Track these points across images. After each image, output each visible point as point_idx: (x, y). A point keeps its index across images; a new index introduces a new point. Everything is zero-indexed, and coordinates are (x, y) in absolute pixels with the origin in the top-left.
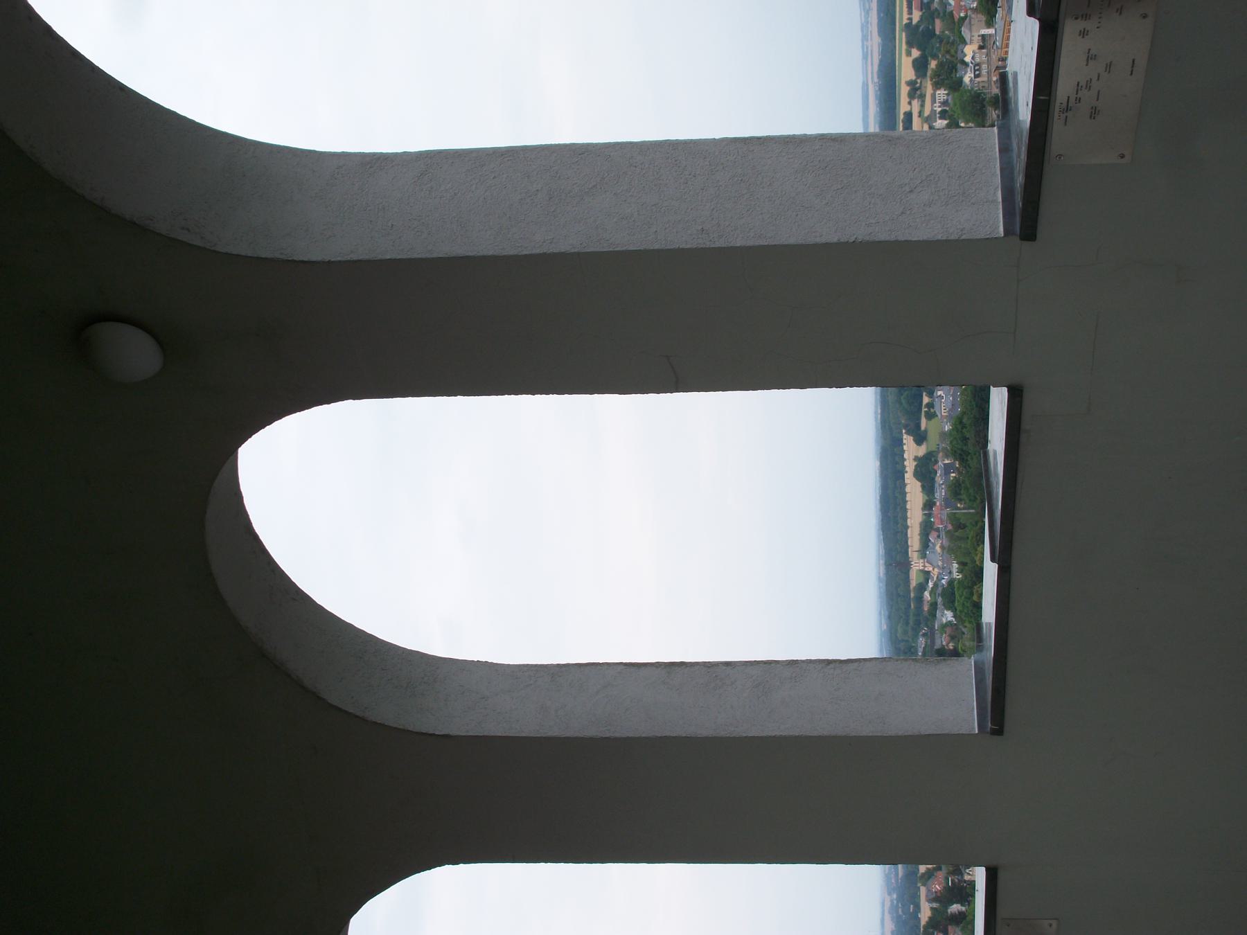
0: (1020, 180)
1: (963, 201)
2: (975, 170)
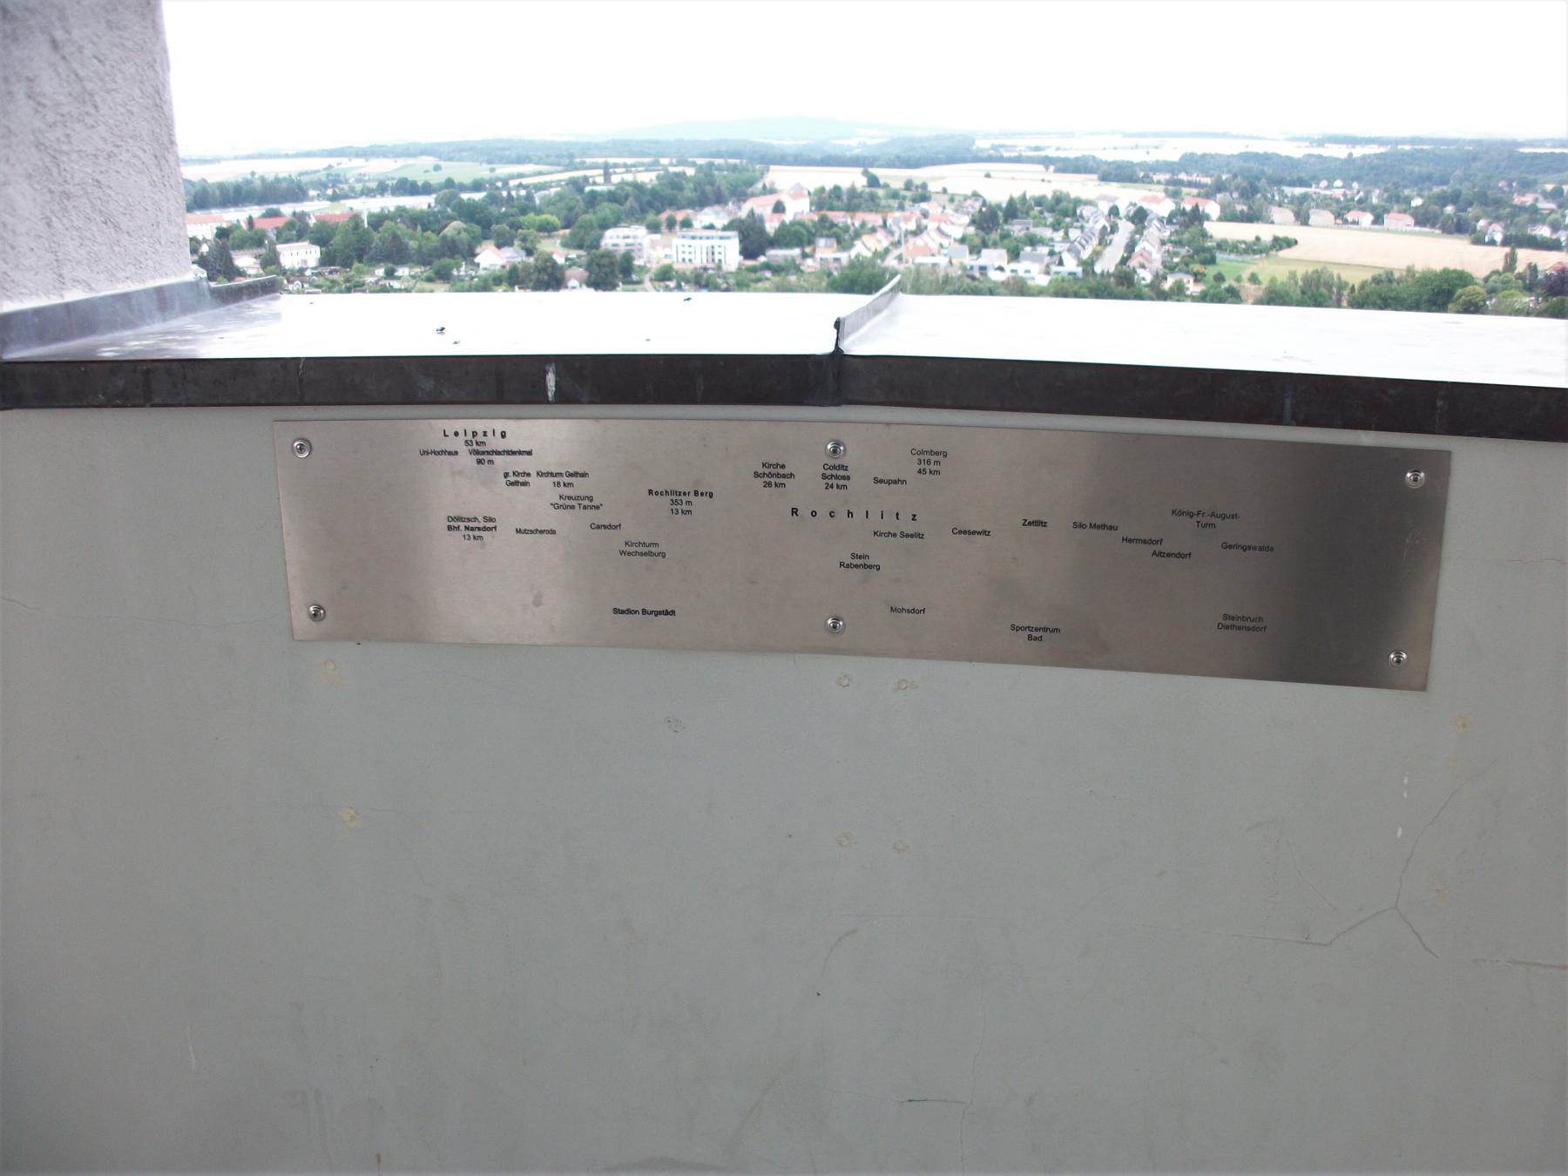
0: (113, 345)
1: (51, 192)
2: (117, 227)
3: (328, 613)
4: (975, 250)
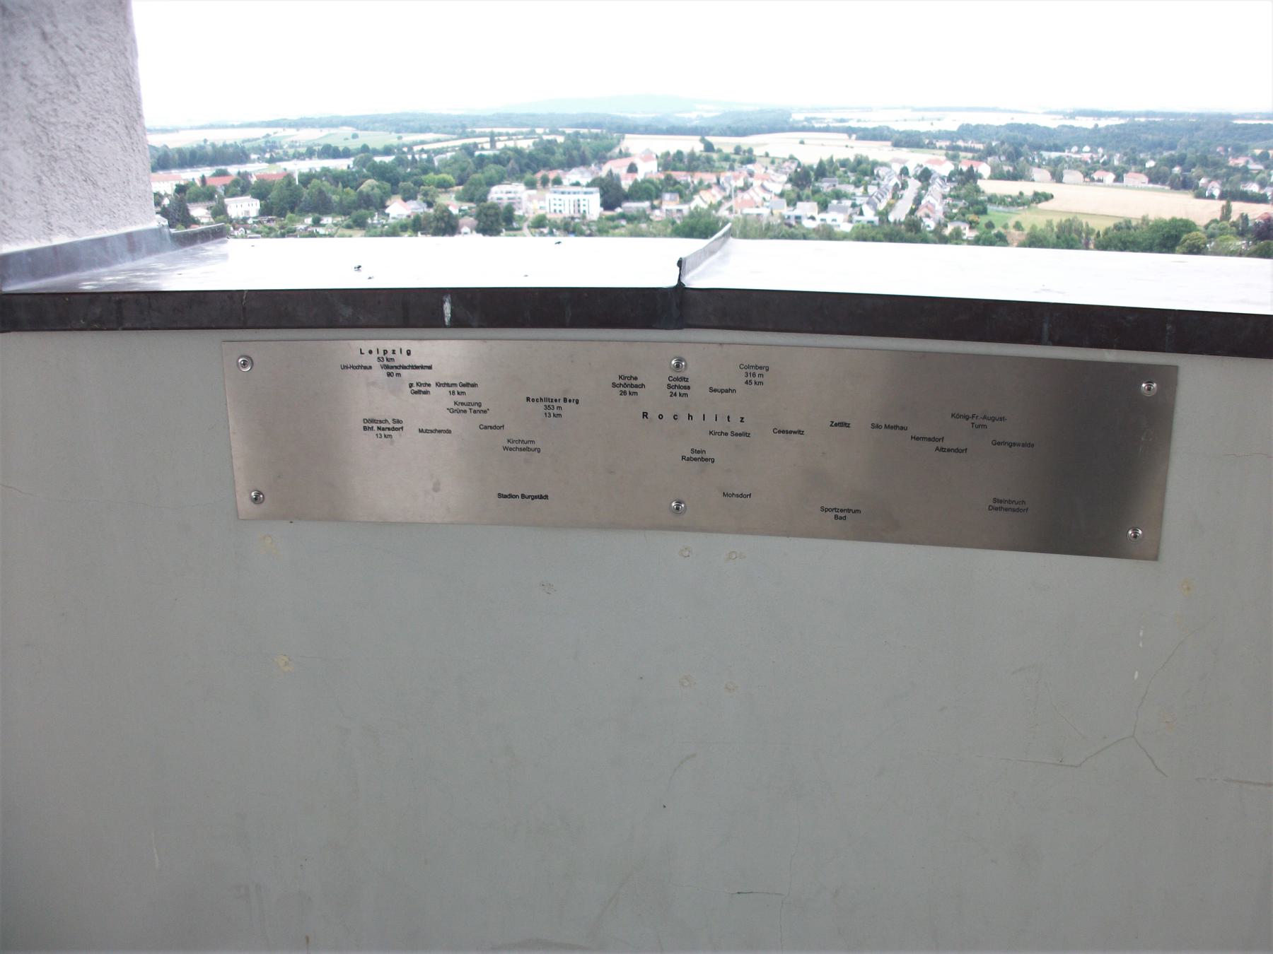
0: (92, 280)
1: (41, 155)
2: (95, 184)
3: (266, 497)
4: (792, 203)
